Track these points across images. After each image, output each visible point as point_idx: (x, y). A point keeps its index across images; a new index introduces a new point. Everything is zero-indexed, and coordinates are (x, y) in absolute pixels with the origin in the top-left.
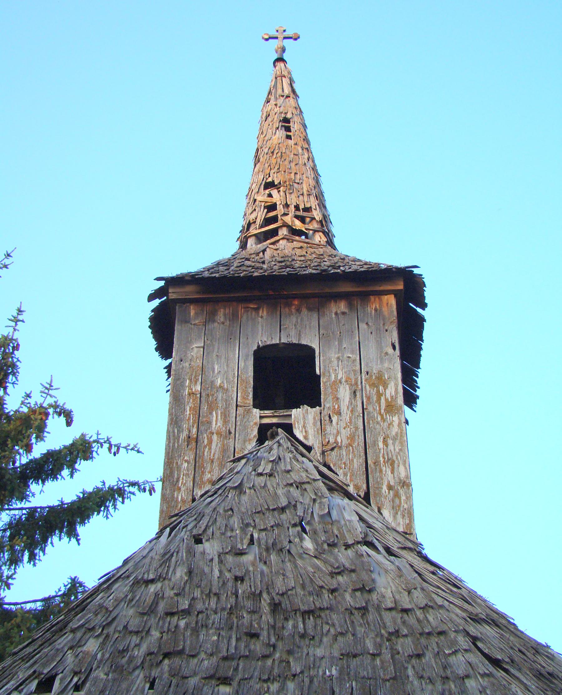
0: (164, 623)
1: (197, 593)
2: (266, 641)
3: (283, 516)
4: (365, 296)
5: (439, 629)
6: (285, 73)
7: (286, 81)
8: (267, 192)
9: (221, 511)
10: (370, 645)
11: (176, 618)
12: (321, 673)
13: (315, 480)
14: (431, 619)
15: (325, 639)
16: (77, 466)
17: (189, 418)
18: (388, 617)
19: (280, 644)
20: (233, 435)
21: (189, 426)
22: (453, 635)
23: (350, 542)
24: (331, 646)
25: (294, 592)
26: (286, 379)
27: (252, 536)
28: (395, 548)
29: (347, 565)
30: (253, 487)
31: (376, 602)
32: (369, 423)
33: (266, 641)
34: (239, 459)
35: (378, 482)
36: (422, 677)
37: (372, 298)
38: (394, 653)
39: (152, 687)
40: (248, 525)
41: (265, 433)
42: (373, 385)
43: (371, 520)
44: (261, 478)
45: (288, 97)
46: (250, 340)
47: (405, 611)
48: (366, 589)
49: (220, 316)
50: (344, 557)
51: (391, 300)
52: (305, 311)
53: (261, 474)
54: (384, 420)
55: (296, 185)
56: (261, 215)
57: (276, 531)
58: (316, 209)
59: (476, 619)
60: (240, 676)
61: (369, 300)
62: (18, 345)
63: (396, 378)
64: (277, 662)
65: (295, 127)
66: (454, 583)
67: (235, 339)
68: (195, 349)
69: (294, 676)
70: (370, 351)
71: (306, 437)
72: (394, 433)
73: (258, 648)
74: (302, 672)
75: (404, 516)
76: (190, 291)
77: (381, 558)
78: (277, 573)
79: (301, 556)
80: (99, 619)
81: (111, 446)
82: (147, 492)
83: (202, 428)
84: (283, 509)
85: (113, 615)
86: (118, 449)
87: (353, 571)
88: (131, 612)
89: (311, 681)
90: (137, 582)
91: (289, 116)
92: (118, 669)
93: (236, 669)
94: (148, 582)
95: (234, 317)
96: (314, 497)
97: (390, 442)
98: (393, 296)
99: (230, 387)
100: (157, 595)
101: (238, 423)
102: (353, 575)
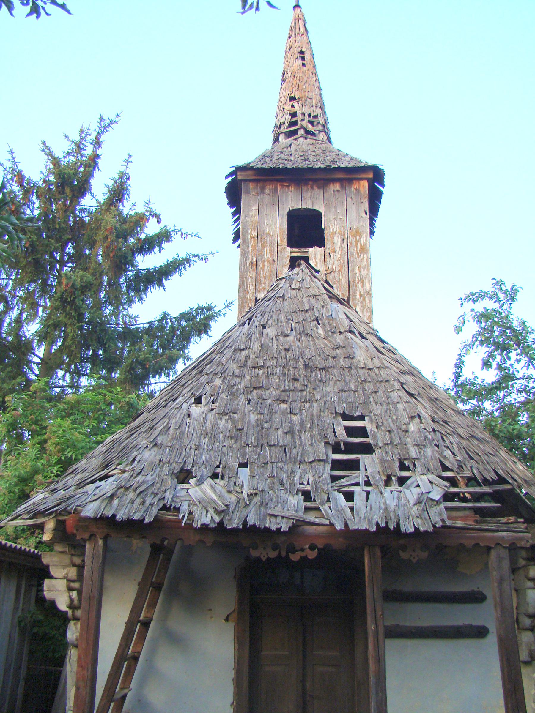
0: (252, 372)
1: (266, 357)
2: (302, 383)
3: (307, 315)
4: (350, 181)
5: (386, 379)
6: (300, 16)
7: (301, 23)
8: (291, 103)
9: (274, 311)
11: (257, 369)
12: (329, 399)
13: (323, 294)
14: (382, 373)
15: (331, 383)
16: (163, 246)
18: (361, 372)
19: (309, 385)
20: (276, 262)
21: (251, 257)
22: (392, 382)
23: (342, 331)
24: (334, 386)
25: (314, 358)
26: (305, 230)
27: (291, 325)
28: (364, 333)
29: (341, 344)
31: (355, 364)
33: (302, 383)
34: (281, 279)
36: (377, 403)
37: (354, 182)
38: (364, 390)
39: (249, 403)
40: (289, 320)
41: (294, 262)
42: (353, 236)
43: (352, 318)
44: (294, 291)
45: (302, 35)
46: (284, 206)
47: (370, 369)
48: (350, 357)
50: (339, 339)
51: (365, 184)
52: (316, 189)
53: (293, 289)
54: (359, 256)
55: (308, 100)
56: (287, 119)
57: (304, 323)
58: (320, 117)
59: (403, 372)
60: (291, 400)
61: (352, 183)
62: (129, 177)
63: (366, 232)
64: (308, 394)
65: (307, 57)
67: (276, 205)
68: (253, 211)
69: (317, 400)
70: (353, 215)
71: (316, 265)
72: (364, 264)
73: (298, 386)
74: (320, 399)
75: (367, 311)
76: (249, 174)
77: (357, 340)
78: (306, 347)
79: (317, 338)
80: (219, 369)
81: (182, 233)
82: (204, 260)
83: (259, 258)
84: (307, 311)
85: (226, 367)
86: (187, 235)
87: (344, 347)
88: (235, 365)
89: (325, 403)
90: (235, 350)
91: (304, 49)
92: (232, 394)
95: (276, 191)
96: (323, 305)
97: (362, 269)
98: (366, 181)
99: (273, 234)
100: (246, 357)
101: (279, 256)
102: (344, 349)
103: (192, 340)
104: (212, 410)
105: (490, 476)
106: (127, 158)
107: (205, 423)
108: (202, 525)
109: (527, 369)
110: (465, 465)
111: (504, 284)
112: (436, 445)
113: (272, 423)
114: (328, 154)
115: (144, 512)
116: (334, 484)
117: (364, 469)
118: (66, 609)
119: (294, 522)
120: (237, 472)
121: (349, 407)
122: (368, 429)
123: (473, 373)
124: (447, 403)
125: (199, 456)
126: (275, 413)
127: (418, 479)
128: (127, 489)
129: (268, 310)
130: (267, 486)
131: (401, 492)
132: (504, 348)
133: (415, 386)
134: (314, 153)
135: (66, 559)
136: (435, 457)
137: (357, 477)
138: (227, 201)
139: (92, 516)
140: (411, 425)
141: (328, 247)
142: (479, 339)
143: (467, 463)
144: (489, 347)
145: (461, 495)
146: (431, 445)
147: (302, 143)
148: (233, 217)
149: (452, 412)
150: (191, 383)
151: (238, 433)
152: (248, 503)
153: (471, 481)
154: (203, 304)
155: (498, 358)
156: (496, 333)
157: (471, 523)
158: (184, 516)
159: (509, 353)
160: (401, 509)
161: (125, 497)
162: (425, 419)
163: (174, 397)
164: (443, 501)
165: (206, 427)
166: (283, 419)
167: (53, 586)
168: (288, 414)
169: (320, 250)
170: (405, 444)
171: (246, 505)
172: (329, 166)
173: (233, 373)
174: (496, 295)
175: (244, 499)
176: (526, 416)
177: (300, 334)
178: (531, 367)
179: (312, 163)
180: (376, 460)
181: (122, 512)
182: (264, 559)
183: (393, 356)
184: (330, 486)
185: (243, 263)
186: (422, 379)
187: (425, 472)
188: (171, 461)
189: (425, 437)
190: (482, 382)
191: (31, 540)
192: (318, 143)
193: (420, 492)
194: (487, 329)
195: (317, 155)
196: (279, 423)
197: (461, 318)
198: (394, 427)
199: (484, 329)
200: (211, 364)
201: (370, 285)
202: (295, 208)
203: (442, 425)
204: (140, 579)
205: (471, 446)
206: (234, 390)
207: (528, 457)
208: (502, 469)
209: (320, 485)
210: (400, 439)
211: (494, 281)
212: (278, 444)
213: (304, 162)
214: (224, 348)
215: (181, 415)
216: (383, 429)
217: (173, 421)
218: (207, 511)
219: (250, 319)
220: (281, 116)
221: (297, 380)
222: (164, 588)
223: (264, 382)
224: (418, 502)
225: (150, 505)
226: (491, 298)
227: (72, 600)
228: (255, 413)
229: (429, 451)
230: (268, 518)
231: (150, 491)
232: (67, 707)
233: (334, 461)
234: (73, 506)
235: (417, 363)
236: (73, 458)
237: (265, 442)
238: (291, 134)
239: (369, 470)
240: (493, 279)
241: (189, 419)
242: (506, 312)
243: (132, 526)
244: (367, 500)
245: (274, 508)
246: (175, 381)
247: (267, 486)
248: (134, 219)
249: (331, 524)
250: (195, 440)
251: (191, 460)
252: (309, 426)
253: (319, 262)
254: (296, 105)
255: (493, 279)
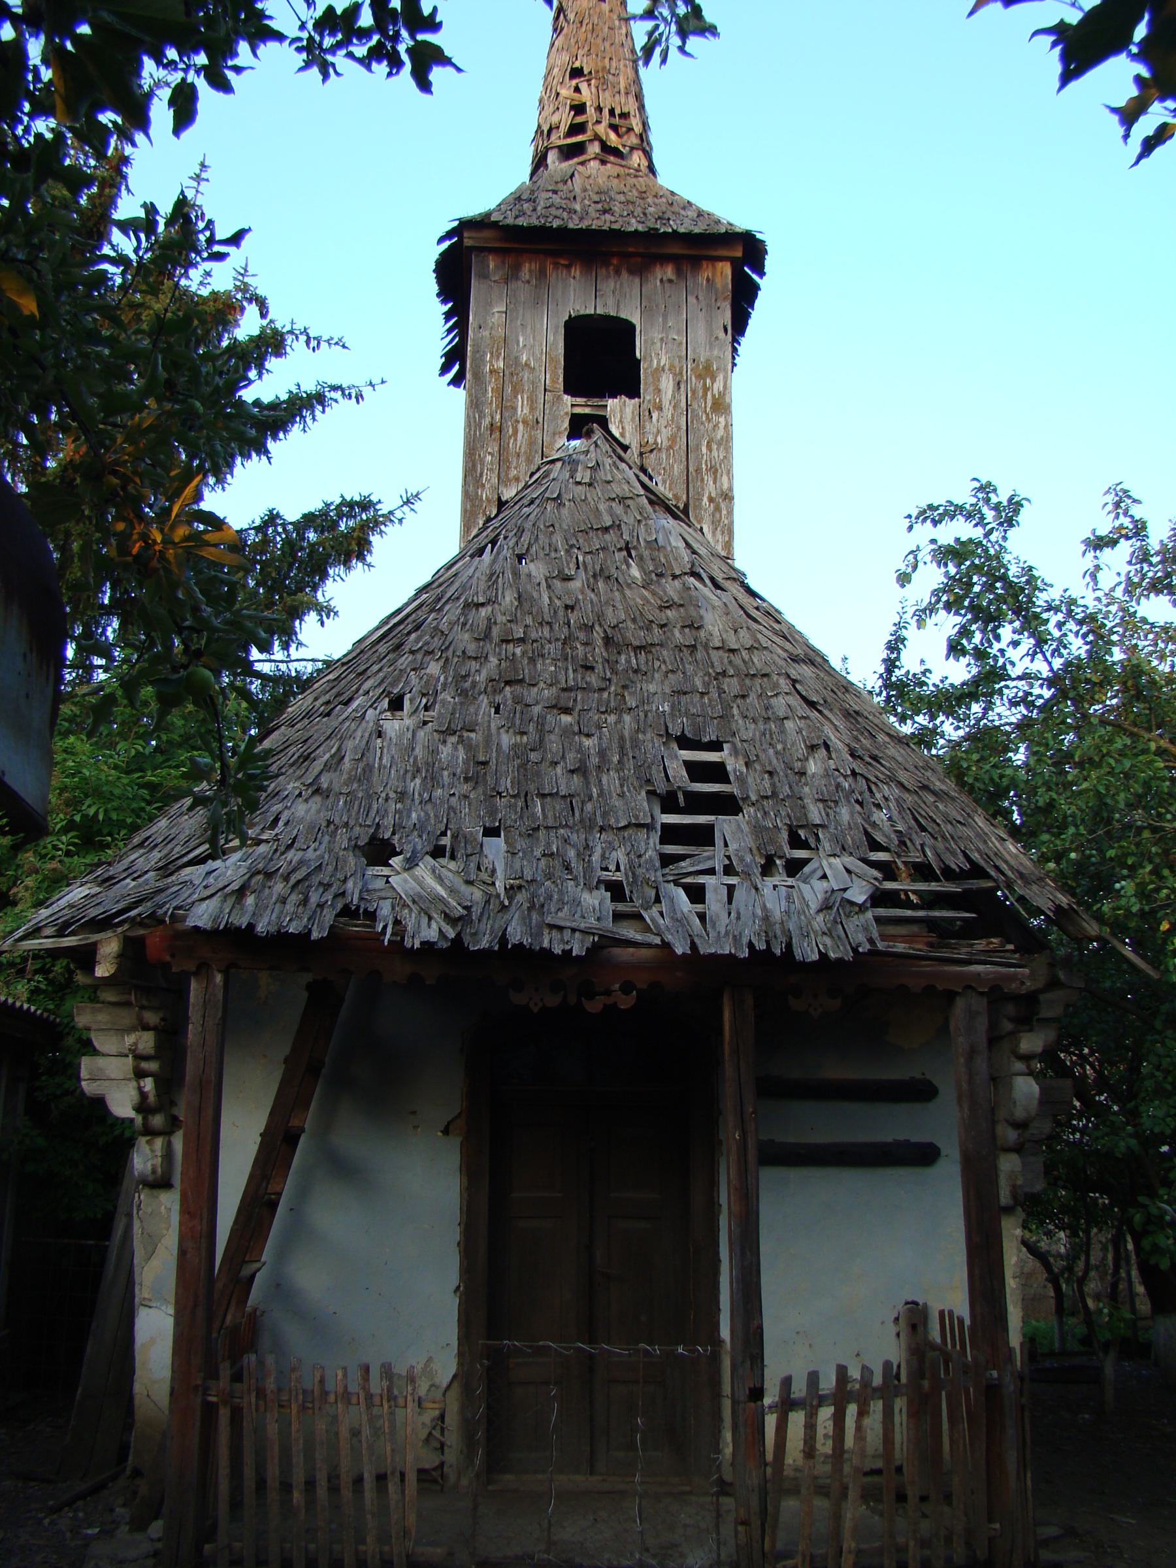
0: (501, 650)
1: (529, 620)
3: (607, 537)
4: (695, 262)
8: (574, 82)
10: (698, 682)
14: (755, 660)
15: (656, 675)
16: (267, 365)
17: (491, 403)
18: (715, 655)
20: (540, 425)
22: (775, 677)
23: (678, 573)
24: (662, 682)
26: (601, 361)
28: (719, 578)
29: (676, 599)
30: (573, 500)
31: (704, 640)
32: (692, 422)
34: (553, 462)
35: (698, 493)
37: (704, 264)
41: (579, 426)
42: (699, 377)
43: (695, 546)
44: (580, 487)
47: (733, 651)
48: (694, 626)
49: (525, 272)
50: (672, 589)
51: (726, 269)
53: (579, 483)
55: (610, 77)
56: (565, 118)
57: (601, 555)
59: (795, 659)
60: (579, 707)
66: (773, 615)
70: (699, 333)
71: (622, 435)
75: (723, 533)
77: (707, 591)
78: (607, 603)
79: (629, 585)
80: (436, 642)
81: (309, 338)
82: (354, 399)
83: (506, 414)
84: (606, 530)
85: (450, 638)
86: (319, 344)
87: (682, 605)
88: (467, 636)
89: (646, 716)
90: (467, 605)
92: (464, 693)
93: (575, 700)
94: (479, 605)
95: (542, 274)
96: (639, 518)
97: (714, 447)
100: (489, 619)
101: (547, 412)
102: (682, 610)
103: (331, 572)
104: (425, 723)
105: (956, 862)
106: (198, 172)
107: (413, 749)
108: (422, 943)
109: (1032, 661)
110: (910, 840)
111: (995, 491)
112: (857, 801)
113: (545, 751)
114: (650, 200)
115: (309, 919)
116: (667, 870)
117: (722, 844)
118: (132, 1114)
119: (596, 939)
120: (482, 845)
121: (693, 724)
122: (729, 768)
123: (922, 661)
124: (876, 721)
125: (405, 814)
126: (550, 732)
127: (825, 863)
128: (269, 875)
129: (528, 525)
130: (540, 871)
131: (792, 887)
132: (989, 619)
133: (818, 687)
134: (622, 198)
135: (127, 1017)
136: (856, 824)
137: (709, 858)
138: (435, 288)
139: (209, 926)
140: (811, 761)
141: (648, 398)
142: (944, 598)
143: (914, 836)
144: (960, 615)
145: (903, 896)
146: (849, 802)
147: (594, 171)
148: (446, 323)
149: (887, 739)
150: (380, 670)
151: (477, 772)
152: (506, 903)
153: (922, 871)
154: (353, 494)
155: (977, 638)
156: (977, 589)
157: (920, 948)
158: (385, 927)
159: (998, 627)
160: (795, 918)
161: (267, 891)
162: (837, 751)
163: (345, 697)
164: (872, 906)
165: (416, 758)
166: (566, 744)
167: (100, 1069)
168: (575, 734)
169: (631, 403)
170: (800, 798)
171: (504, 908)
172: (651, 229)
173: (464, 652)
174: (980, 512)
175: (498, 896)
176: (1022, 750)
177: (594, 576)
178: (1039, 656)
179: (620, 219)
180: (745, 828)
181: (266, 920)
182: (535, 1010)
183: (776, 626)
184: (659, 873)
185: (472, 425)
186: (830, 672)
187: (838, 851)
188: (352, 823)
189: (838, 786)
190: (942, 681)
191: (19, 987)
192: (629, 175)
193: (829, 890)
194: (960, 580)
195: (628, 202)
196: (557, 752)
197: (911, 557)
198: (779, 766)
199: (955, 580)
200: (419, 632)
201: (730, 480)
202: (582, 312)
203: (870, 764)
204: (286, 1050)
205: (923, 805)
206: (467, 685)
207: (1024, 830)
208: (979, 850)
209: (639, 871)
210: (790, 787)
211: (978, 485)
212: (557, 793)
213: (603, 217)
214: (443, 600)
215: (364, 732)
216: (758, 767)
217: (349, 745)
218: (430, 918)
219: (494, 542)
220: (551, 109)
221: (592, 668)
222: (324, 1071)
223: (526, 672)
224: (826, 907)
225: (318, 905)
226: (969, 517)
227: (143, 1095)
228: (511, 730)
229: (844, 813)
230: (546, 931)
231: (315, 880)
232: (137, 1300)
233: (665, 826)
234: (169, 907)
235: (818, 640)
236: (101, 817)
237: (532, 787)
238: (571, 152)
239: (733, 846)
240: (974, 479)
241: (379, 740)
242: (996, 547)
243: (286, 948)
244: (730, 901)
245: (556, 913)
246: (343, 664)
247: (540, 871)
248: (210, 308)
249: (666, 945)
250: (394, 782)
251: (389, 821)
252: (616, 759)
253: (629, 428)
254: (584, 87)
255: (974, 479)
